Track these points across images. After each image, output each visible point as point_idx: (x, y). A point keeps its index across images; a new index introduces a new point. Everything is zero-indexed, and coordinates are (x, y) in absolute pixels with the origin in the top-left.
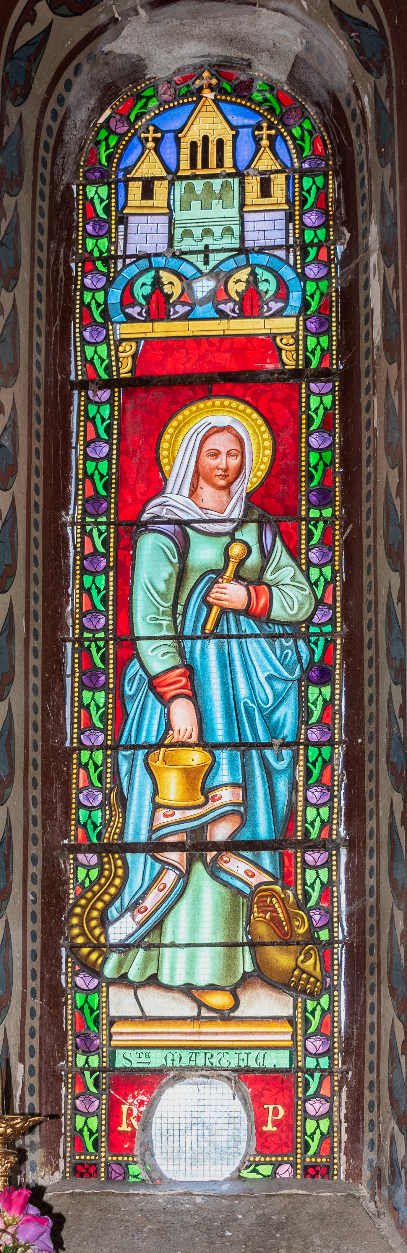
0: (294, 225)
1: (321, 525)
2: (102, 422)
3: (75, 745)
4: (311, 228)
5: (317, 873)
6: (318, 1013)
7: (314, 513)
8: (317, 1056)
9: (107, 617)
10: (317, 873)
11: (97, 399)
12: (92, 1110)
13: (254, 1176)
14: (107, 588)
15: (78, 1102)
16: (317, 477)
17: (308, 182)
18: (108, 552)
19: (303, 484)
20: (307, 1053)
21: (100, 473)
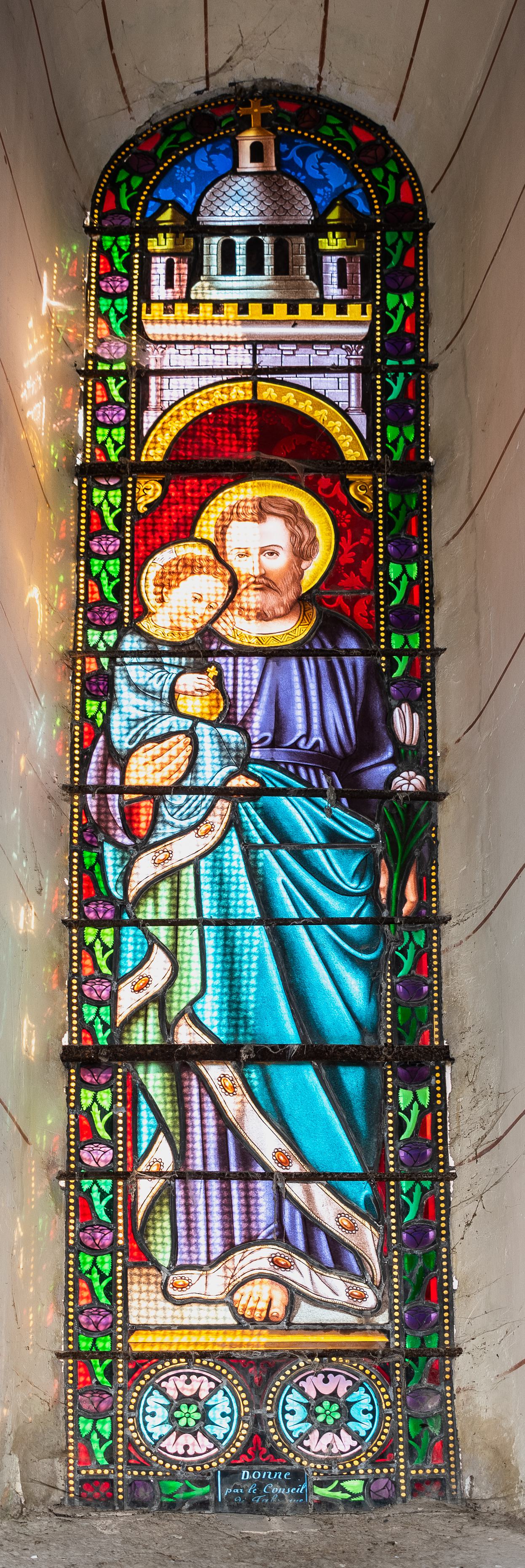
1: (401, 377)
3: (75, 917)
5: (415, 1094)
6: (399, 247)
7: (397, 641)
10: (415, 1094)
13: (339, 1495)
14: (113, 1272)
15: (86, 987)
16: (400, 594)
18: (128, 402)
19: (381, 545)
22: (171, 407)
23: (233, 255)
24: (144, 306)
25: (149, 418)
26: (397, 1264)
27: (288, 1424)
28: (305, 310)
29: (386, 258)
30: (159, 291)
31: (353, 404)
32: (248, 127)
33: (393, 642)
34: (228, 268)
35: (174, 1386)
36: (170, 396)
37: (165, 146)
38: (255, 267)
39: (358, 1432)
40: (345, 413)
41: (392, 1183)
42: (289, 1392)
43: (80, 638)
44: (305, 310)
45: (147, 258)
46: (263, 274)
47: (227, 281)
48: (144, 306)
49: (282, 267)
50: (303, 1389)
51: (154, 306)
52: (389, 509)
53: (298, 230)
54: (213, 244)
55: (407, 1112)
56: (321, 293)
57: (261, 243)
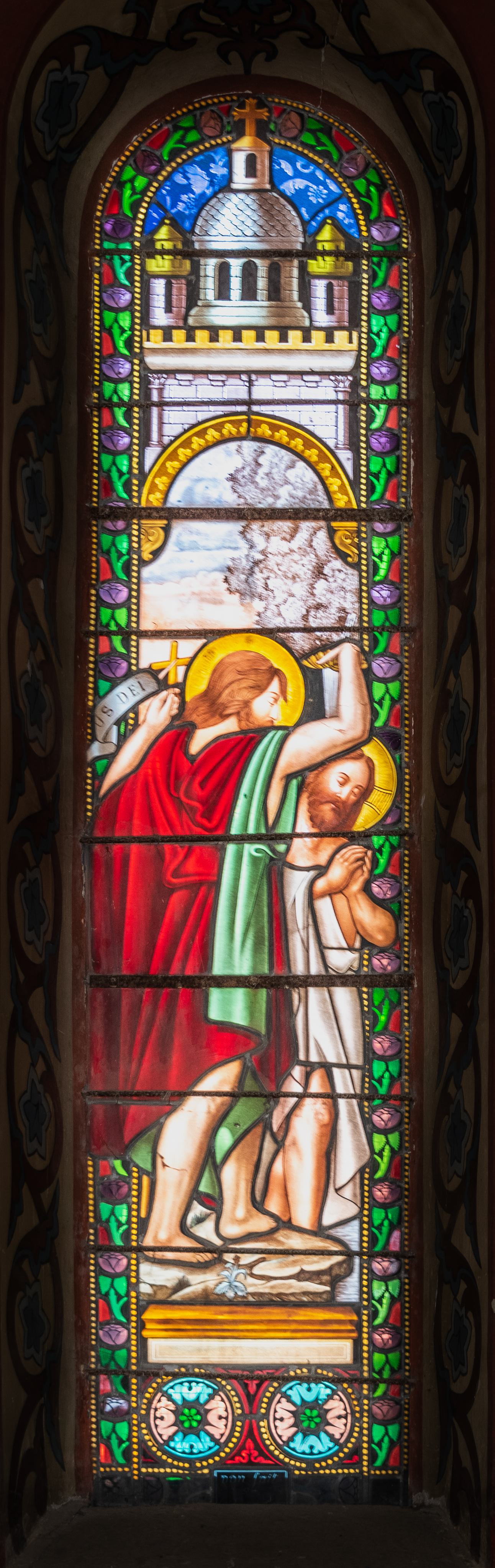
0: (360, 332)
2: (120, 1444)
4: (381, 1058)
8: (383, 384)
9: (132, 293)
11: (110, 1270)
12: (119, 1269)
17: (379, 1288)
20: (371, 380)
21: (117, 1293)
23: (228, 276)
24: (144, 333)
25: (151, 454)
28: (295, 336)
30: (160, 317)
32: (241, 134)
34: (223, 292)
35: (181, 1391)
36: (171, 431)
37: (170, 145)
41: (365, 1250)
43: (135, 539)
44: (295, 336)
45: (147, 278)
48: (144, 333)
49: (275, 292)
53: (288, 254)
54: (210, 266)
56: (311, 321)
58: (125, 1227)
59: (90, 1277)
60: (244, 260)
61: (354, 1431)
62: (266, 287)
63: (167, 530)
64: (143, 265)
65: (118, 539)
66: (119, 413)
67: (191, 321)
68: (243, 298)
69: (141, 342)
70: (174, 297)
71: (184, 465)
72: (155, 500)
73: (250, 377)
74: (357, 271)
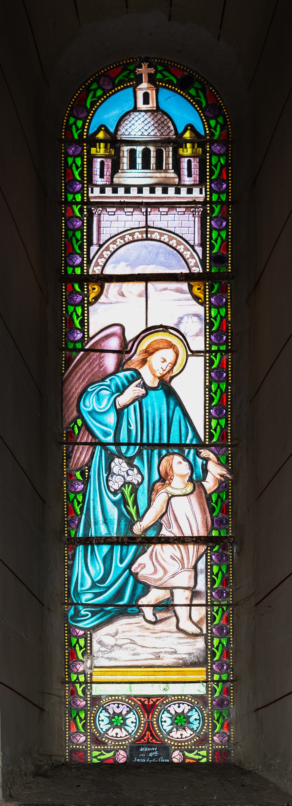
0: (206, 188)
1: (219, 355)
22: (104, 244)
25: (94, 249)
26: (208, 159)
27: (164, 727)
29: (212, 173)
30: (98, 180)
31: (197, 242)
33: (213, 197)
34: (133, 165)
38: (146, 165)
39: (193, 728)
40: (192, 247)
42: (163, 713)
45: (91, 159)
46: (150, 169)
47: (133, 173)
50: (169, 710)
51: (95, 189)
52: (212, 317)
55: (215, 430)
57: (149, 151)
58: (80, 169)
59: (64, 450)
60: (143, 147)
61: (206, 131)
62: (155, 156)
63: (102, 288)
64: (89, 151)
65: (76, 196)
66: (76, 209)
67: (116, 180)
68: (143, 168)
69: (87, 194)
70: (105, 170)
71: (112, 254)
72: (97, 271)
73: (147, 236)
74: (204, 152)
